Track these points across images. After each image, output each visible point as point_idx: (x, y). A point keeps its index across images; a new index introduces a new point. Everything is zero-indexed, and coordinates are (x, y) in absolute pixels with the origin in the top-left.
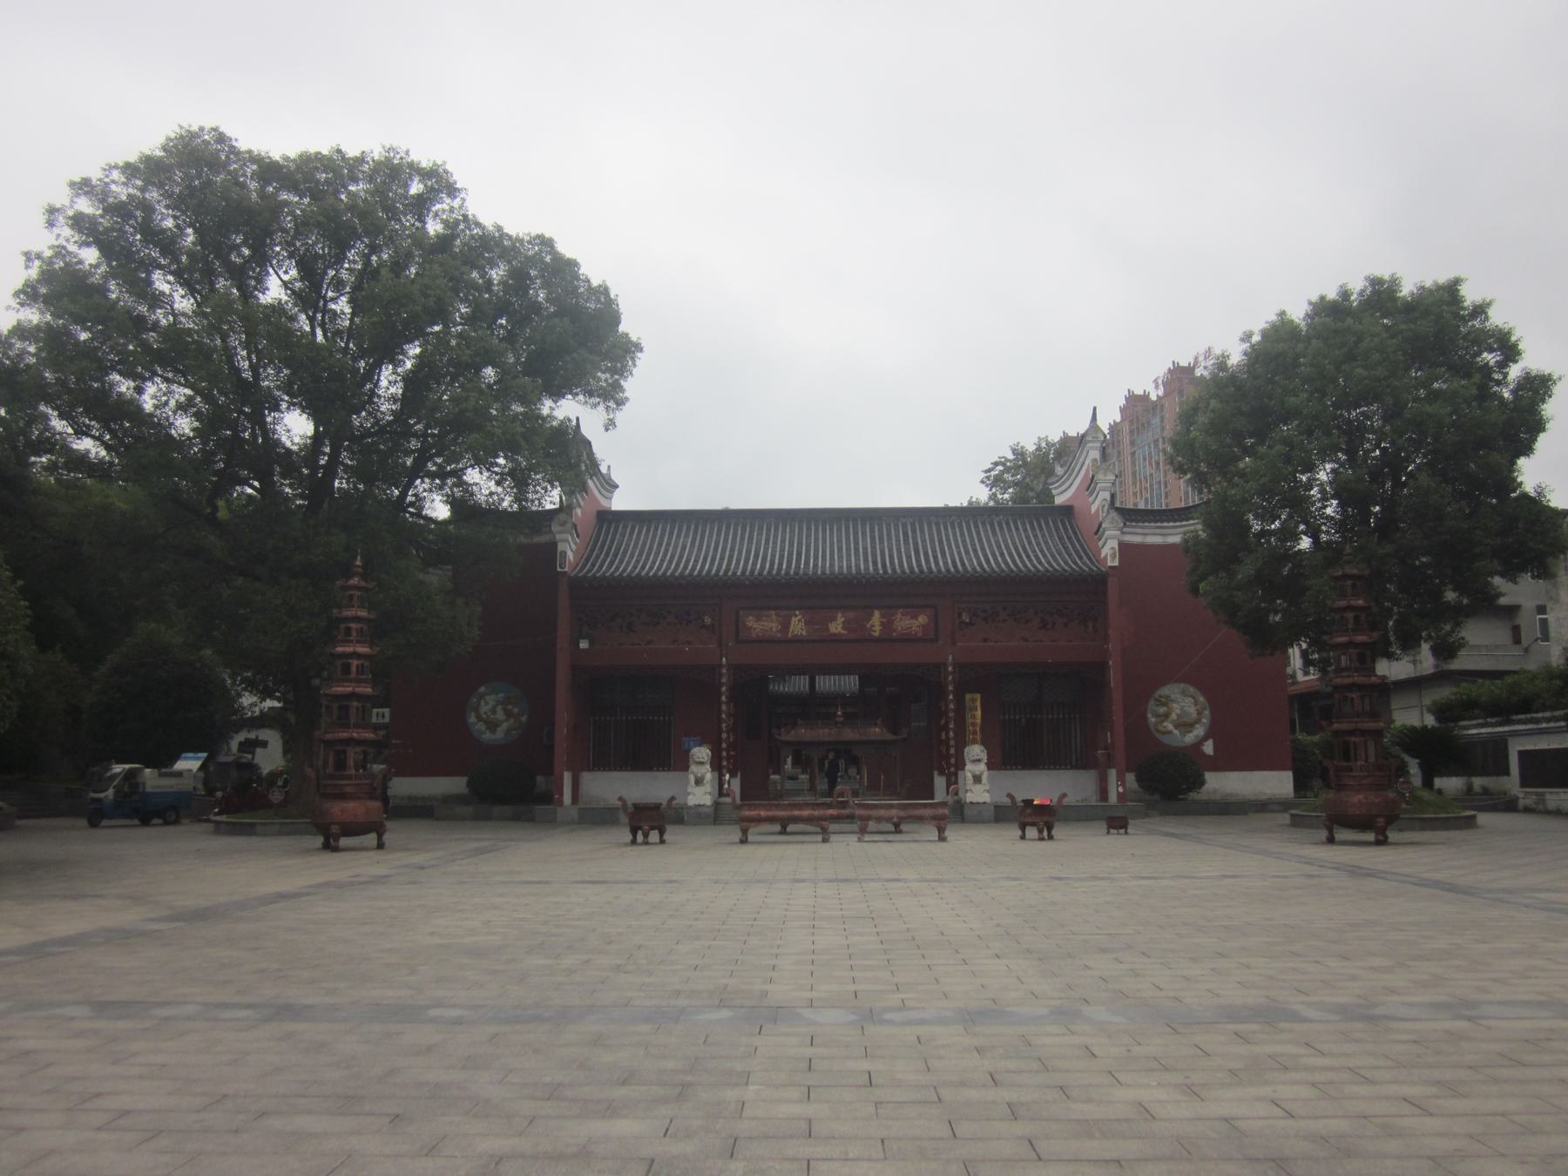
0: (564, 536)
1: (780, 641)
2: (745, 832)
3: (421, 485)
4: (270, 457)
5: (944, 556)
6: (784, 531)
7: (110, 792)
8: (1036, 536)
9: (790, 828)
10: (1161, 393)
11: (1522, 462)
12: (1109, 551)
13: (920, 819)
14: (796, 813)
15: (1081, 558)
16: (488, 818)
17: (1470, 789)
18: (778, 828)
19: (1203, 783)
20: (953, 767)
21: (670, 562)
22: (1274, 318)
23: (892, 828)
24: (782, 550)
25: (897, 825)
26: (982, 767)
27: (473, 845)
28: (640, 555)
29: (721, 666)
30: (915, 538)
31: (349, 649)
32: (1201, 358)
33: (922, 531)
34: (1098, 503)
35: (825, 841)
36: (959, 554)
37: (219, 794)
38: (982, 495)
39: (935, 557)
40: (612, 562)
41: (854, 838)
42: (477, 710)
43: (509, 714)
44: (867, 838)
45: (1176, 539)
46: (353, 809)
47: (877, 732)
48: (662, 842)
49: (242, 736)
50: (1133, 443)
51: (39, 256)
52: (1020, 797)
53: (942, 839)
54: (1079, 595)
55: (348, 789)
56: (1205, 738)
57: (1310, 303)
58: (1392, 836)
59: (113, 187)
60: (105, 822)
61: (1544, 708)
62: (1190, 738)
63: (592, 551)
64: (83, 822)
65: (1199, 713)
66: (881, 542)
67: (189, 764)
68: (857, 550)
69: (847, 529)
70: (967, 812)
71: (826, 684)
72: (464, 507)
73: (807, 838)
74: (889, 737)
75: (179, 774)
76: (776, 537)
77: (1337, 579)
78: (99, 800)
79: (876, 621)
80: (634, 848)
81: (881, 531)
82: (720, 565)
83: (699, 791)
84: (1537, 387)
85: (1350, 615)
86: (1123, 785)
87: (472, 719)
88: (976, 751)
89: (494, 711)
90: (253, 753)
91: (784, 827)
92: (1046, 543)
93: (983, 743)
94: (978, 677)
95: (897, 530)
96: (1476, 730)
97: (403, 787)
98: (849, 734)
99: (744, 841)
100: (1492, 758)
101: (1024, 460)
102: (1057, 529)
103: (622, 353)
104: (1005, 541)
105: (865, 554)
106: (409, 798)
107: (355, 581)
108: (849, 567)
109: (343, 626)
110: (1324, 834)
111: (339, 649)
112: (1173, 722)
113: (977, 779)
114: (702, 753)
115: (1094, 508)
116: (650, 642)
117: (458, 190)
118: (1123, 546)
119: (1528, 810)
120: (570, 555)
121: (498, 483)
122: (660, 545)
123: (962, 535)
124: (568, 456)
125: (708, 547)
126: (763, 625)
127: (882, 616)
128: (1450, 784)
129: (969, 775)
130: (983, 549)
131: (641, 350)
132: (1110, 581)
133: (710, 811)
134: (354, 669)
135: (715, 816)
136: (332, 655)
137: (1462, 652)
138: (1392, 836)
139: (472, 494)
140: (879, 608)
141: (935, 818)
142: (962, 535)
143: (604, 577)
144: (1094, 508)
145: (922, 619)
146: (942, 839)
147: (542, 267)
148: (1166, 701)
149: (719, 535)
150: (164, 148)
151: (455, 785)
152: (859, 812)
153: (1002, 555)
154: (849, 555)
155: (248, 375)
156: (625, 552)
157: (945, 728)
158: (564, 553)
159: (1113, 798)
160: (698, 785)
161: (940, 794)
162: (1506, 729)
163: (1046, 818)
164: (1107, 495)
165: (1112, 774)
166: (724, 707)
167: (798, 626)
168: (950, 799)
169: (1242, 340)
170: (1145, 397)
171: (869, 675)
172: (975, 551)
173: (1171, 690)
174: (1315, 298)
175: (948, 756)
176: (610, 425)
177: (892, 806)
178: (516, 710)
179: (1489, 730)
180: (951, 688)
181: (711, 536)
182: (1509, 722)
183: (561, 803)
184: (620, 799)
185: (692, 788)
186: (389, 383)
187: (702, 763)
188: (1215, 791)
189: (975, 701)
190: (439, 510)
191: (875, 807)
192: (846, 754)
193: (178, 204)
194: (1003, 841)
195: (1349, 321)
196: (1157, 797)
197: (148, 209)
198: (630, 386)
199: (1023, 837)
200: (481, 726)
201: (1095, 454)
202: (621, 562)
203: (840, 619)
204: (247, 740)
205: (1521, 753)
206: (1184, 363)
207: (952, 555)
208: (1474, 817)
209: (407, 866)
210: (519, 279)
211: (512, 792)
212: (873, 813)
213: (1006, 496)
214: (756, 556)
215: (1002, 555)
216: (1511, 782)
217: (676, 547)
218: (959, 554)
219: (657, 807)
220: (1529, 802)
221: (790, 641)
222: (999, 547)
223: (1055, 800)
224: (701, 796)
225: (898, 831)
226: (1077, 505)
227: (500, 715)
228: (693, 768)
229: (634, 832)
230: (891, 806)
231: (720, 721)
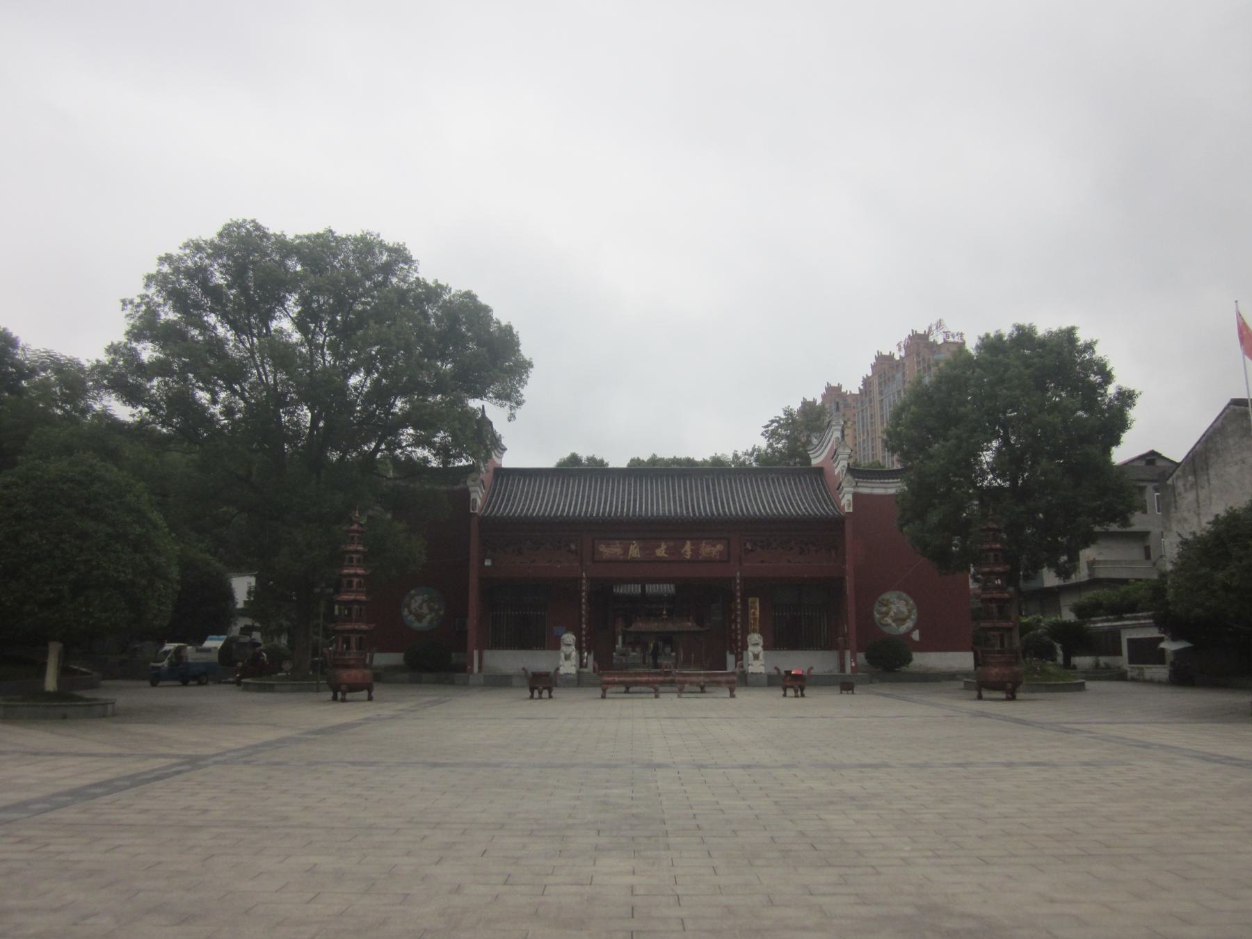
2: (604, 691)
7: (165, 663)
9: (631, 689)
10: (903, 354)
11: (1114, 449)
12: (846, 501)
13: (718, 683)
14: (638, 679)
17: (1097, 665)
18: (623, 689)
19: (911, 660)
20: (740, 649)
23: (699, 689)
25: (702, 688)
26: (759, 649)
27: (427, 699)
31: (352, 571)
32: (934, 328)
34: (840, 467)
35: (657, 697)
37: (240, 664)
42: (408, 606)
43: (431, 610)
45: (892, 491)
47: (690, 625)
48: (550, 697)
50: (881, 393)
51: (131, 302)
53: (732, 696)
54: (824, 531)
55: (352, 662)
58: (1019, 696)
60: (161, 683)
61: (1143, 610)
62: (903, 629)
64: (147, 683)
65: (910, 611)
67: (214, 643)
70: (749, 679)
71: (651, 589)
74: (697, 628)
75: (208, 650)
77: (983, 530)
78: (158, 668)
79: (688, 547)
83: (568, 663)
84: (1126, 398)
85: (991, 554)
87: (406, 612)
88: (755, 638)
89: (420, 607)
93: (761, 633)
96: (1101, 624)
98: (671, 627)
99: (603, 697)
100: (1109, 644)
103: (522, 367)
108: (670, 511)
111: (346, 571)
113: (756, 657)
114: (569, 638)
115: (837, 471)
118: (856, 496)
119: (1133, 680)
120: (479, 501)
124: (482, 438)
126: (610, 550)
128: (1083, 661)
135: (579, 681)
140: (691, 539)
141: (727, 682)
144: (837, 471)
145: (719, 547)
146: (732, 696)
147: (470, 312)
148: (886, 604)
152: (677, 678)
157: (735, 621)
158: (475, 500)
159: (848, 670)
161: (731, 668)
165: (848, 653)
167: (634, 551)
168: (737, 670)
170: (891, 357)
174: (982, 335)
175: (736, 641)
176: (511, 417)
177: (700, 674)
182: (1121, 619)
185: (562, 662)
191: (689, 675)
192: (667, 638)
194: (771, 699)
195: (1001, 356)
199: (785, 695)
200: (412, 618)
203: (664, 547)
205: (1130, 641)
206: (921, 332)
208: (1083, 684)
211: (436, 663)
212: (688, 679)
213: (780, 446)
216: (1123, 661)
219: (547, 675)
220: (1134, 674)
221: (628, 561)
223: (806, 670)
224: (568, 667)
225: (703, 691)
226: (825, 466)
227: (425, 610)
228: (563, 648)
229: (532, 691)
230: (700, 675)
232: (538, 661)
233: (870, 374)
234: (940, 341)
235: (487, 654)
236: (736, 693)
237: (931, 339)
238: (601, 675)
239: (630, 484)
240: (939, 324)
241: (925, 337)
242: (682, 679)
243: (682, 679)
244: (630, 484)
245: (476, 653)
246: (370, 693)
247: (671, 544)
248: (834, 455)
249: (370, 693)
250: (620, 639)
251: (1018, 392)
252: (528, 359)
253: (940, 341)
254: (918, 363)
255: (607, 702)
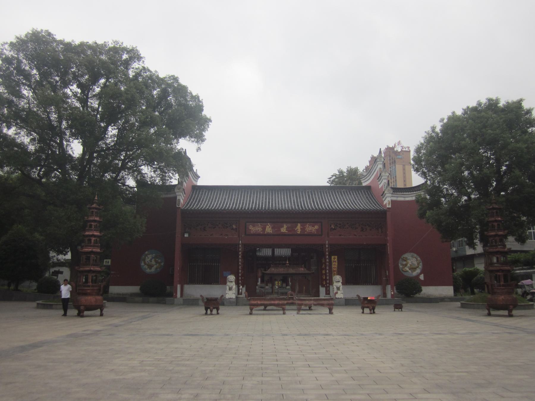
0: (179, 193)
1: (262, 235)
2: (251, 310)
3: (123, 173)
4: (65, 158)
5: (324, 204)
6: (263, 194)
8: (357, 197)
14: (273, 302)
15: (375, 205)
16: (148, 302)
19: (421, 291)
21: (220, 204)
22: (451, 114)
24: (263, 200)
26: (340, 284)
28: (209, 202)
29: (239, 244)
30: (312, 197)
31: (91, 233)
32: (397, 145)
33: (315, 194)
34: (382, 184)
35: (284, 313)
36: (330, 203)
38: (328, 185)
39: (321, 204)
40: (198, 204)
41: (295, 312)
42: (144, 260)
43: (157, 262)
44: (301, 312)
45: (414, 198)
46: (91, 299)
47: (302, 270)
48: (218, 314)
49: (52, 270)
52: (362, 296)
54: (376, 218)
55: (89, 291)
56: (420, 274)
57: (463, 109)
59: (5, 51)
62: (415, 274)
63: (190, 200)
65: (418, 264)
66: (300, 198)
68: (291, 201)
69: (287, 193)
71: (279, 252)
72: (141, 183)
73: (275, 312)
76: (260, 196)
80: (206, 316)
81: (299, 195)
82: (239, 206)
83: (231, 292)
85: (496, 224)
86: (393, 291)
87: (143, 264)
90: (57, 277)
91: (265, 307)
92: (362, 199)
94: (336, 250)
95: (305, 194)
97: (114, 290)
98: (291, 271)
99: (251, 314)
101: (343, 174)
102: (365, 194)
103: (204, 122)
104: (346, 198)
105: (294, 202)
106: (118, 294)
107: (94, 206)
108: (288, 207)
109: (89, 224)
110: (486, 312)
111: (87, 233)
112: (408, 267)
114: (232, 278)
116: (212, 235)
117: (141, 58)
120: (182, 201)
121: (154, 172)
122: (216, 198)
123: (330, 196)
124: (182, 163)
125: (234, 199)
126: (255, 229)
127: (301, 226)
129: (335, 287)
130: (338, 201)
131: (211, 121)
132: (388, 213)
133: (235, 300)
134: (93, 241)
135: (237, 303)
136: (84, 235)
137: (528, 241)
138: (514, 312)
139: (144, 177)
140: (300, 222)
141: (328, 305)
142: (330, 196)
143: (195, 210)
145: (316, 227)
146: (331, 313)
147: (174, 88)
148: (405, 260)
149: (238, 195)
150: (26, 36)
151: (135, 289)
153: (346, 203)
154: (288, 203)
155: (55, 124)
156: (203, 200)
160: (230, 290)
162: (531, 271)
163: (373, 305)
164: (386, 181)
166: (240, 260)
167: (269, 229)
169: (440, 121)
171: (295, 249)
172: (335, 202)
173: (408, 255)
175: (326, 280)
178: (159, 261)
179: (525, 271)
180: (327, 254)
181: (235, 195)
183: (176, 297)
184: (201, 296)
185: (227, 291)
186: (112, 131)
187: (232, 282)
188: (424, 294)
189: (335, 259)
190: (131, 182)
191: (305, 300)
193: (31, 59)
196: (403, 295)
197: (19, 62)
198: (206, 134)
199: (363, 313)
200: (146, 267)
201: (380, 166)
202: (201, 204)
203: (285, 227)
204: (55, 271)
206: (391, 146)
207: (327, 203)
209: (110, 325)
210: (164, 94)
211: (157, 292)
212: (304, 302)
214: (253, 203)
215: (346, 203)
217: (222, 199)
218: (330, 203)
219: (216, 299)
221: (265, 235)
222: (344, 200)
224: (231, 295)
225: (310, 309)
226: (372, 185)
227: (153, 262)
228: (228, 283)
229: (206, 309)
230: (311, 300)
231: (238, 266)
232: (212, 291)
233: (368, 165)
234: (399, 150)
235: (186, 287)
236: (333, 311)
237: (395, 149)
238: (249, 300)
239: (266, 194)
240: (399, 143)
241: (393, 148)
242: (299, 302)
243: (299, 302)
244: (266, 194)
245: (179, 287)
246: (101, 311)
247: (289, 225)
248: (379, 178)
249: (101, 311)
250: (259, 279)
251: (498, 131)
252: (208, 117)
253: (399, 150)
254: (390, 160)
255: (253, 317)
